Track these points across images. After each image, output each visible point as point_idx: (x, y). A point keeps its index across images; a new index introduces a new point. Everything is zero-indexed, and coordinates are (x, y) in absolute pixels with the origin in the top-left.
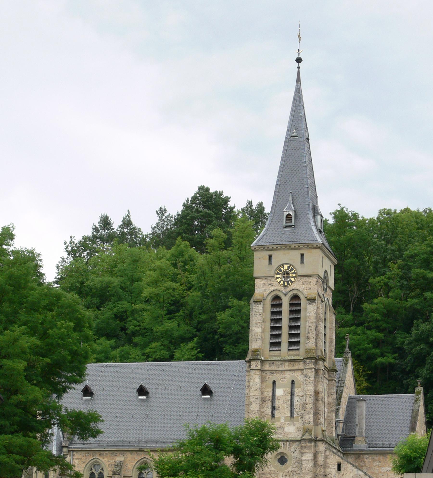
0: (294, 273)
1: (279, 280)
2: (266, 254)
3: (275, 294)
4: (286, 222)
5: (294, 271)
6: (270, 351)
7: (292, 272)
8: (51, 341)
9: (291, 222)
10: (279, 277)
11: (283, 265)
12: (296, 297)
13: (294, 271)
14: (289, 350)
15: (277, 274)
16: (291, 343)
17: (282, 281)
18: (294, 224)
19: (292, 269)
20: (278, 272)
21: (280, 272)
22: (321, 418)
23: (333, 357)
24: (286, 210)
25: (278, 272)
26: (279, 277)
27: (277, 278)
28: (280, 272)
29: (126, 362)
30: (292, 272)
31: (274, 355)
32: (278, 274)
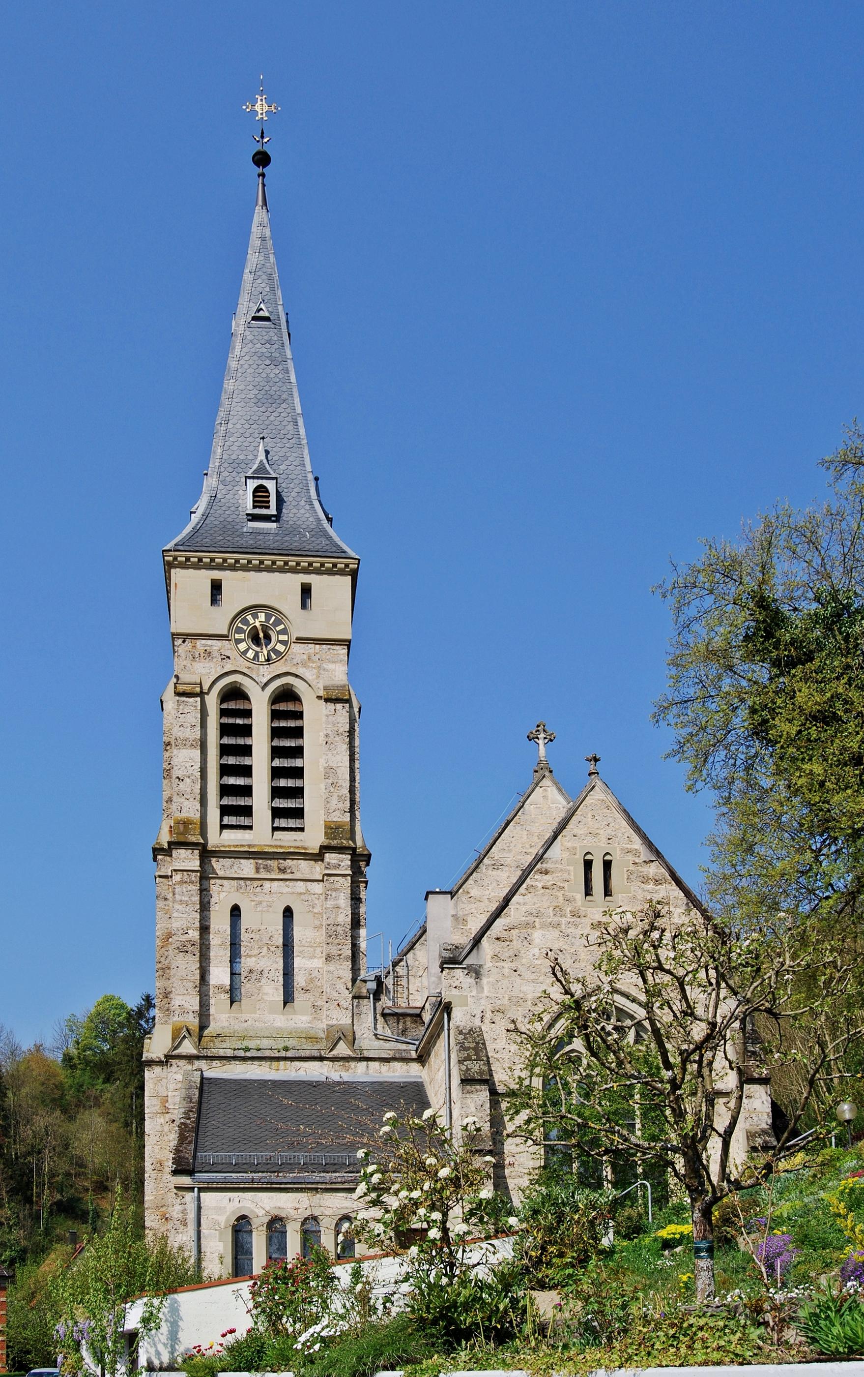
0: (284, 632)
1: (242, 646)
2: (205, 577)
3: (235, 682)
4: (254, 507)
5: (282, 627)
6: (275, 829)
7: (278, 628)
8: (332, 968)
9: (268, 507)
10: (243, 640)
11: (254, 609)
12: (287, 695)
13: (282, 627)
14: (275, 829)
15: (236, 632)
16: (277, 813)
17: (251, 651)
18: (275, 513)
19: (278, 622)
20: (240, 625)
21: (245, 628)
22: (738, 1162)
23: (626, 882)
24: (254, 473)
25: (240, 625)
26: (243, 640)
27: (238, 641)
28: (245, 628)
29: (334, 1172)
30: (278, 628)
31: (233, 839)
32: (239, 631)
